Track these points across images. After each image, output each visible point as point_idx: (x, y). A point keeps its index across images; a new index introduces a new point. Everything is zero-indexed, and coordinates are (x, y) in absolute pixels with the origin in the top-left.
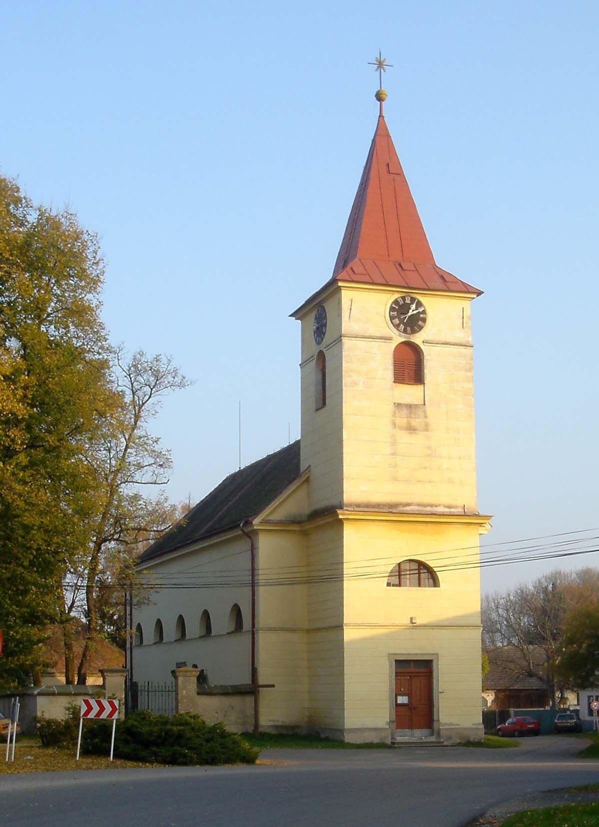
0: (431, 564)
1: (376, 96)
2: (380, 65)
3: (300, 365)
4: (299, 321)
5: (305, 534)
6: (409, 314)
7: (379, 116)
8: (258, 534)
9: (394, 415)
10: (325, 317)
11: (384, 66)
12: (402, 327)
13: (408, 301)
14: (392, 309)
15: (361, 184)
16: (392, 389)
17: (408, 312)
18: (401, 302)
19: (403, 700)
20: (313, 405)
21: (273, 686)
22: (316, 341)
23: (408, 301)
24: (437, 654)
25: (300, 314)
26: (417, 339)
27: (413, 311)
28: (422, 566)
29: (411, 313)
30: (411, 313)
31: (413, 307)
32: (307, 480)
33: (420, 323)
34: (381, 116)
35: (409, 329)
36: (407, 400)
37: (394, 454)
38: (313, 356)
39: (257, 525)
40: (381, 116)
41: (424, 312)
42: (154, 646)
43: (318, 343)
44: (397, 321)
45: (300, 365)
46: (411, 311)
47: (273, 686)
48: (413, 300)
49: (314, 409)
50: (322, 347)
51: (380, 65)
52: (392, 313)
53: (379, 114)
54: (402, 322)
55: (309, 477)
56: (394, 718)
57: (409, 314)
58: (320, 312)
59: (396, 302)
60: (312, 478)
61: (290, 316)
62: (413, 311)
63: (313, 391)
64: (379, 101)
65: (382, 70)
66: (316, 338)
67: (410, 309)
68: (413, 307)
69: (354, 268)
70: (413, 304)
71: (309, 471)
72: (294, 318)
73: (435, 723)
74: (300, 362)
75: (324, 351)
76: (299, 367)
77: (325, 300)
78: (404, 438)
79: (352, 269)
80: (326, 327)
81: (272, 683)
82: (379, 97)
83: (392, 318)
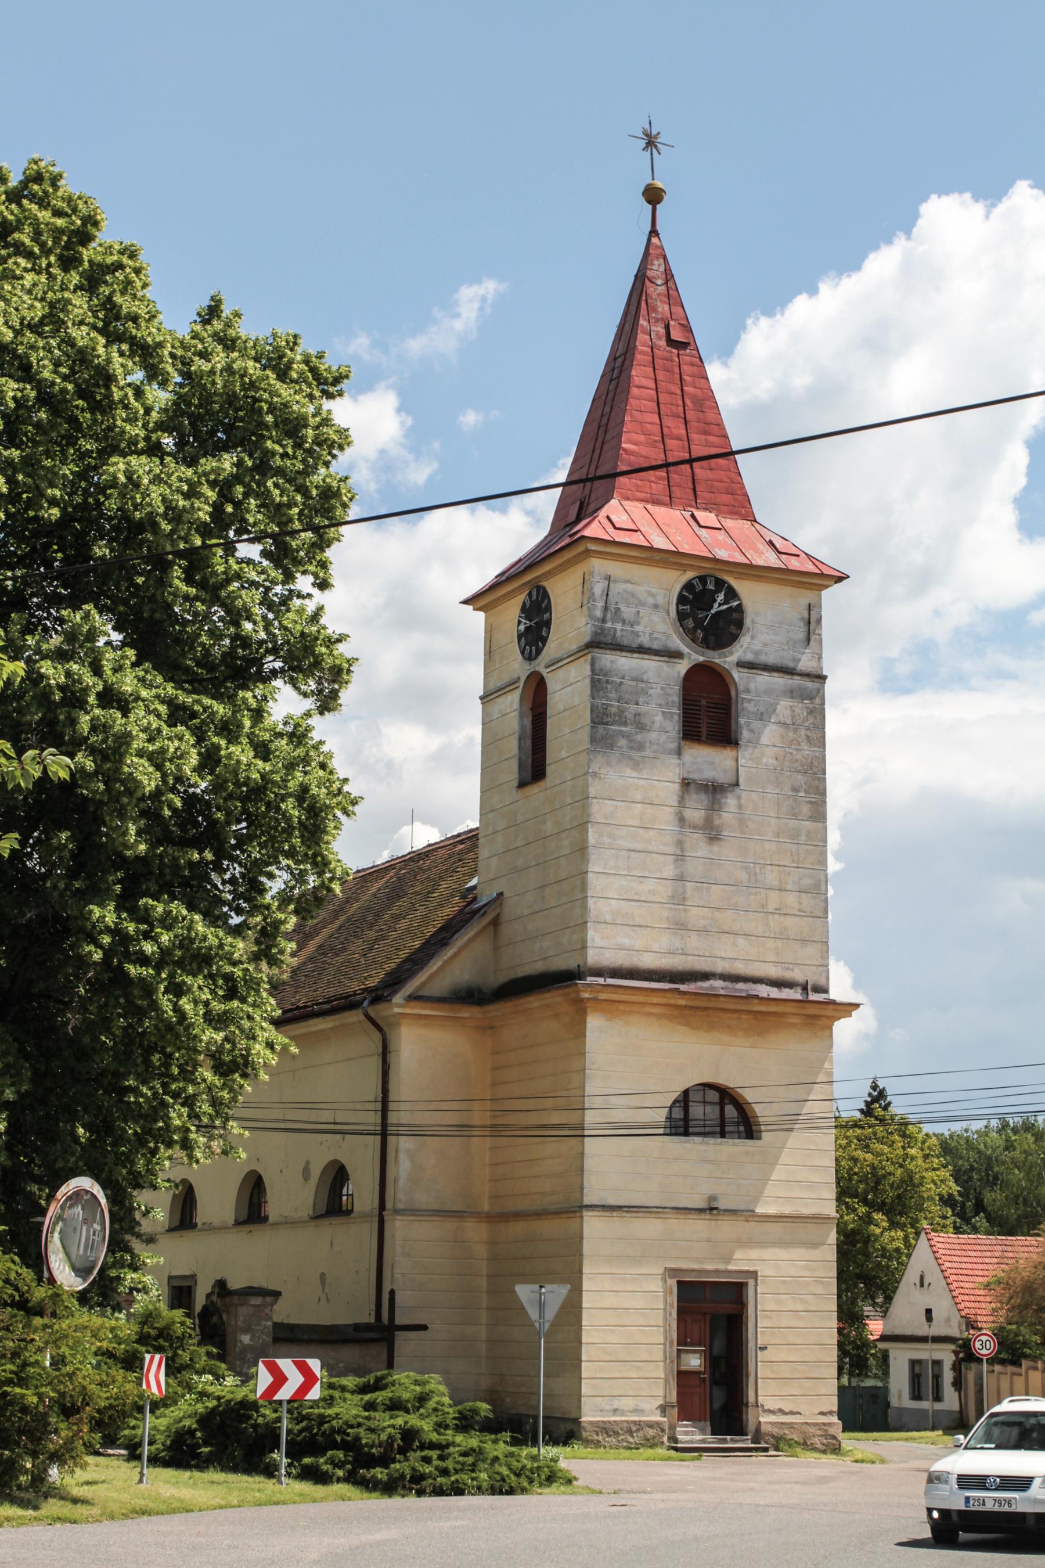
0: (749, 1095)
1: (644, 193)
2: (651, 142)
3: (481, 698)
4: (481, 615)
5: (489, 1028)
6: (713, 611)
7: (651, 233)
8: (399, 1024)
9: (682, 800)
10: (548, 609)
11: (659, 146)
12: (700, 634)
13: (711, 587)
14: (681, 600)
15: (613, 358)
16: (679, 753)
17: (712, 607)
18: (699, 587)
19: (694, 1362)
20: (511, 773)
21: (424, 1328)
22: (523, 653)
23: (711, 587)
24: (754, 1274)
25: (482, 602)
26: (728, 659)
27: (720, 605)
28: (726, 1095)
29: (715, 608)
30: (715, 608)
31: (721, 597)
32: (496, 923)
33: (733, 629)
34: (654, 232)
35: (712, 639)
36: (708, 774)
37: (681, 878)
38: (516, 682)
39: (399, 1006)
40: (654, 232)
41: (740, 609)
42: (312, 1223)
43: (530, 658)
44: (690, 623)
45: (481, 698)
46: (716, 605)
47: (424, 1328)
48: (720, 583)
49: (515, 783)
50: (540, 665)
51: (651, 142)
52: (681, 607)
53: (649, 228)
54: (699, 625)
55: (498, 915)
56: (673, 1398)
57: (713, 611)
58: (534, 598)
59: (689, 586)
60: (504, 917)
61: (466, 602)
62: (720, 605)
63: (512, 747)
64: (649, 202)
65: (654, 150)
66: (525, 648)
67: (715, 601)
68: (721, 597)
69: (613, 518)
70: (720, 592)
71: (501, 904)
72: (471, 607)
73: (751, 1411)
74: (482, 694)
75: (544, 672)
76: (479, 701)
77: (549, 575)
78: (698, 847)
79: (608, 518)
80: (549, 628)
81: (423, 1323)
82: (653, 196)
83: (681, 616)
